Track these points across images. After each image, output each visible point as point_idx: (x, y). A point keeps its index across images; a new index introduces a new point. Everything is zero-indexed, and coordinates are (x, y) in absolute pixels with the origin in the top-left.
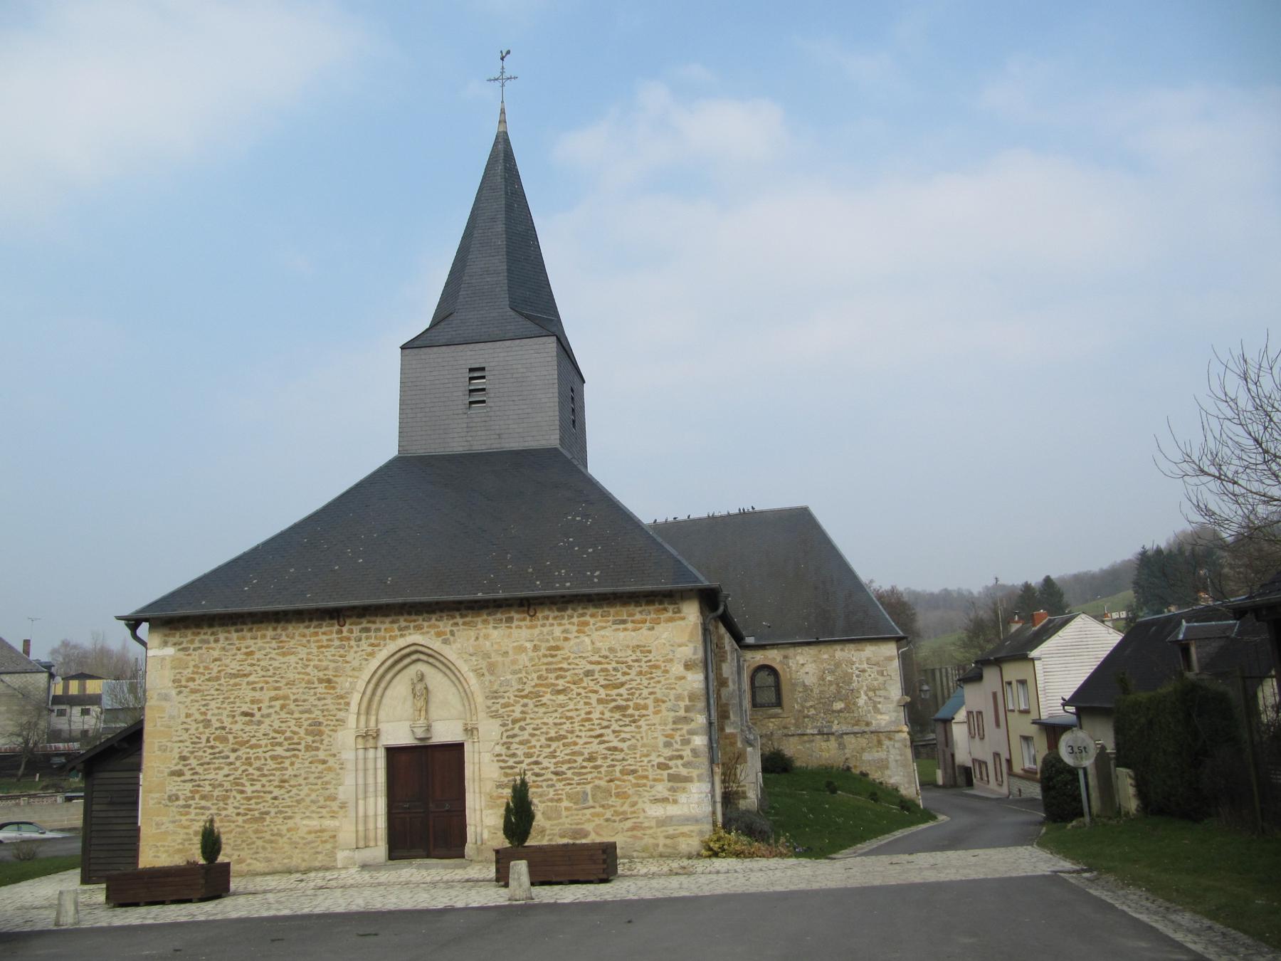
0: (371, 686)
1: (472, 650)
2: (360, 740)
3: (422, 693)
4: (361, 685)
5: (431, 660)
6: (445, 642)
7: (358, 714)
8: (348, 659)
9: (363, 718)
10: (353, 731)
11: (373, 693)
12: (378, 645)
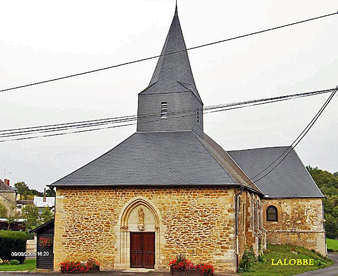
3: (142, 215)
7: (121, 221)
9: (123, 222)
12: (128, 199)
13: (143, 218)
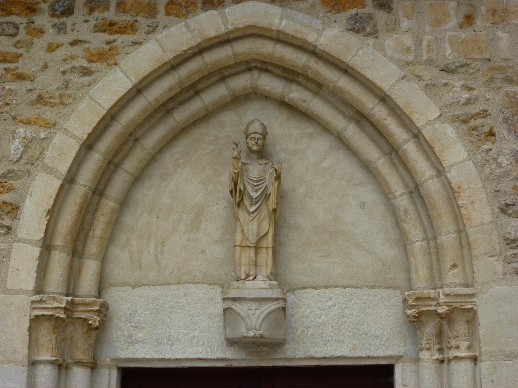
0: (95, 161)
1: (449, 54)
2: (46, 335)
3: (261, 198)
4: (61, 151)
5: (296, 94)
6: (351, 18)
7: (47, 247)
8: (23, 66)
9: (59, 260)
10: (23, 302)
11: (98, 191)
12: (131, 28)
13: (277, 218)
